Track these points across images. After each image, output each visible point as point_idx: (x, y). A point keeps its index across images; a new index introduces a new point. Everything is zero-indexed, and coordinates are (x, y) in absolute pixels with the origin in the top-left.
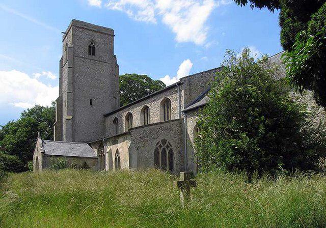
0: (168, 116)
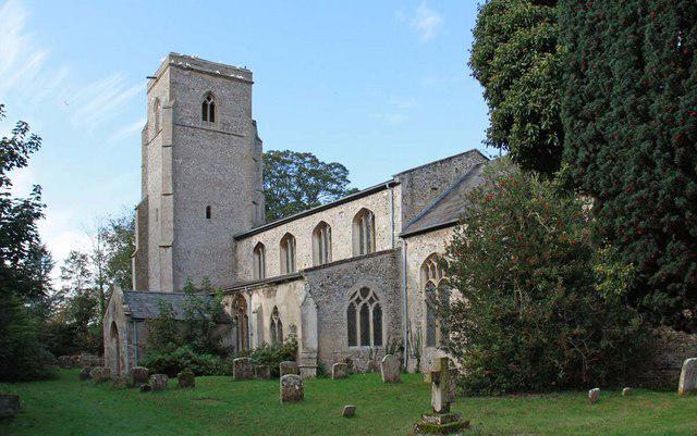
0: (369, 244)
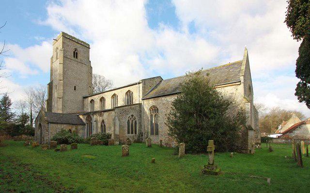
0: (130, 101)
